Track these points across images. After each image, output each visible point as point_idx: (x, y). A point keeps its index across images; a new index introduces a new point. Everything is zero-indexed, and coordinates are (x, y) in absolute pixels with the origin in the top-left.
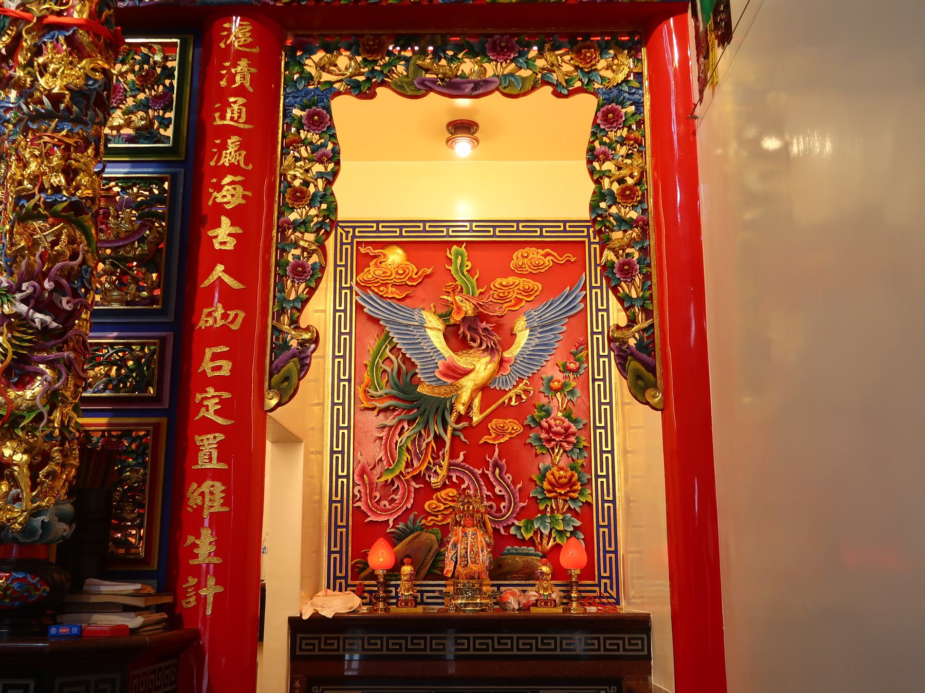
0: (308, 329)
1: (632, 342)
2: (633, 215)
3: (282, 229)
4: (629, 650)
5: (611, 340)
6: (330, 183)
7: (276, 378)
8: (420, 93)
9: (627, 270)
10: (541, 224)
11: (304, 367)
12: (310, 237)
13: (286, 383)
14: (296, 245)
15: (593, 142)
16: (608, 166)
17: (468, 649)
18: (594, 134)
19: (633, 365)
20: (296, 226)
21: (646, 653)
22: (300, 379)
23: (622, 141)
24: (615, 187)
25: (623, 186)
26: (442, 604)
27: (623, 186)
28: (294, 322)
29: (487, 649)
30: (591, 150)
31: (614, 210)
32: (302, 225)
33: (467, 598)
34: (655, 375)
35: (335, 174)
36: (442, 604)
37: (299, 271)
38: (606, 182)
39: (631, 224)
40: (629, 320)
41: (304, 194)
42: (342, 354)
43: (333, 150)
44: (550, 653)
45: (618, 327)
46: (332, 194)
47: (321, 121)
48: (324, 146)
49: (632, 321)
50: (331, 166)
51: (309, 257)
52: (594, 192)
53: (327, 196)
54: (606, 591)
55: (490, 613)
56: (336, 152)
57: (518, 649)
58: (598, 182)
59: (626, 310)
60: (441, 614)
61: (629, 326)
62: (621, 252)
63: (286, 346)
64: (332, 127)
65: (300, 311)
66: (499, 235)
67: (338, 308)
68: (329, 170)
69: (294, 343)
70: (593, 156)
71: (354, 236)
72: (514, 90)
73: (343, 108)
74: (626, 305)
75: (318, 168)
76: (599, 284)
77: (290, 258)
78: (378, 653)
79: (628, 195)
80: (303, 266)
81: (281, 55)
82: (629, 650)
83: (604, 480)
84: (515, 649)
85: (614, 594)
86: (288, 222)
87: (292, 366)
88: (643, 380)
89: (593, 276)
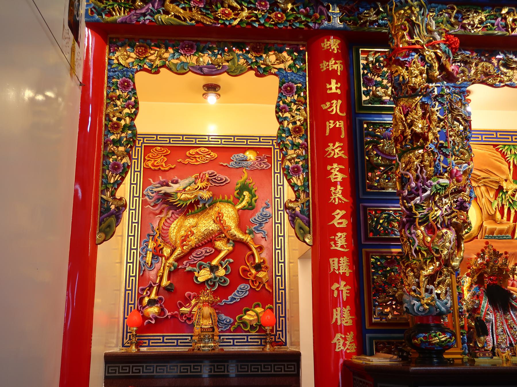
0: (121, 199)
1: (298, 210)
2: (301, 141)
3: (106, 145)
4: (269, 365)
5: (286, 208)
6: (133, 120)
7: (104, 225)
8: (185, 71)
9: (296, 171)
10: (247, 138)
11: (118, 219)
12: (121, 149)
13: (108, 229)
14: (113, 153)
15: (279, 102)
16: (287, 115)
17: (133, 367)
18: (280, 98)
19: (298, 221)
20: (114, 142)
21: (107, 365)
22: (116, 227)
23: (294, 102)
24: (291, 126)
25: (294, 126)
26: (191, 346)
27: (294, 126)
28: (113, 195)
29: (281, 371)
30: (278, 106)
31: (290, 138)
32: (117, 143)
33: (205, 343)
34: (309, 227)
35: (136, 114)
36: (191, 346)
37: (116, 167)
38: (286, 123)
39: (299, 146)
40: (296, 197)
41: (118, 126)
42: (134, 208)
43: (135, 101)
44: (221, 373)
45: (291, 201)
46: (135, 126)
47: (128, 85)
48: (130, 99)
49: (298, 198)
50: (134, 110)
51: (121, 160)
52: (279, 129)
53: (132, 127)
54: (279, 338)
55: (217, 351)
56: (136, 103)
57: (275, 371)
58: (281, 123)
59: (295, 192)
60: (189, 352)
61: (296, 201)
62: (293, 161)
63: (109, 209)
64: (134, 89)
65: (116, 189)
66: (224, 144)
67: (132, 182)
68: (132, 112)
69: (113, 207)
70: (279, 109)
71: (143, 143)
72: (236, 72)
73: (141, 79)
74: (296, 189)
75: (127, 111)
76: (279, 171)
77: (111, 160)
78: (270, 373)
79: (297, 130)
80: (118, 165)
81: (105, 49)
82: (269, 365)
83: (280, 278)
84: (249, 371)
85: (284, 340)
86: (109, 140)
87: (113, 219)
88: (303, 230)
89: (276, 168)
